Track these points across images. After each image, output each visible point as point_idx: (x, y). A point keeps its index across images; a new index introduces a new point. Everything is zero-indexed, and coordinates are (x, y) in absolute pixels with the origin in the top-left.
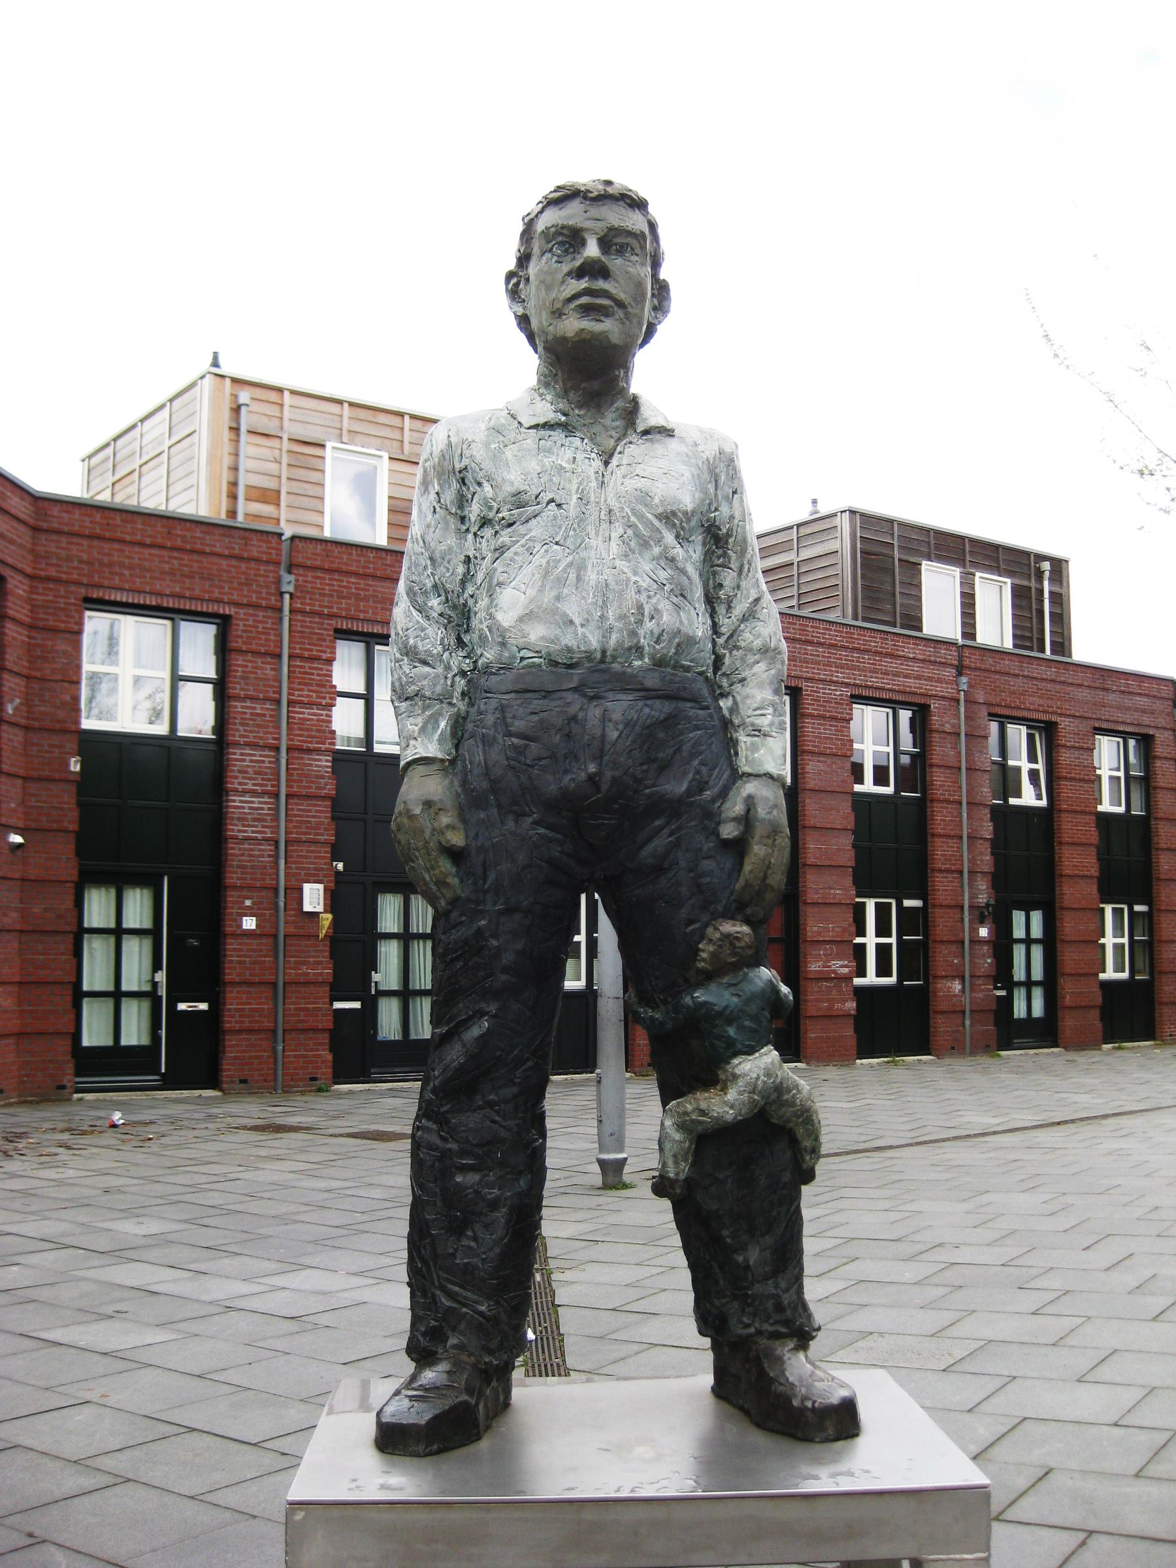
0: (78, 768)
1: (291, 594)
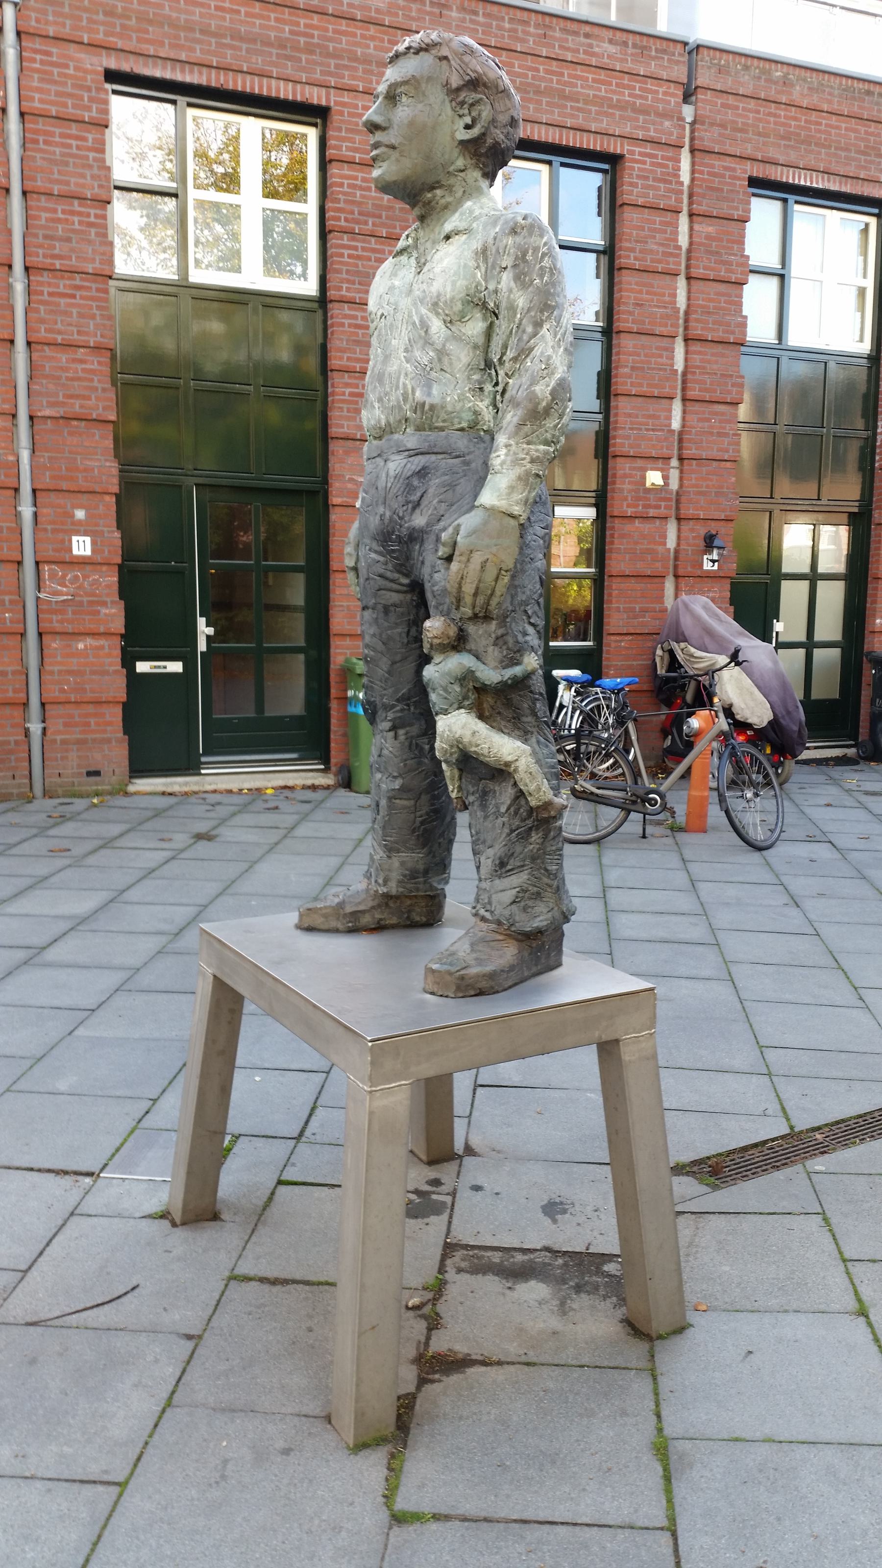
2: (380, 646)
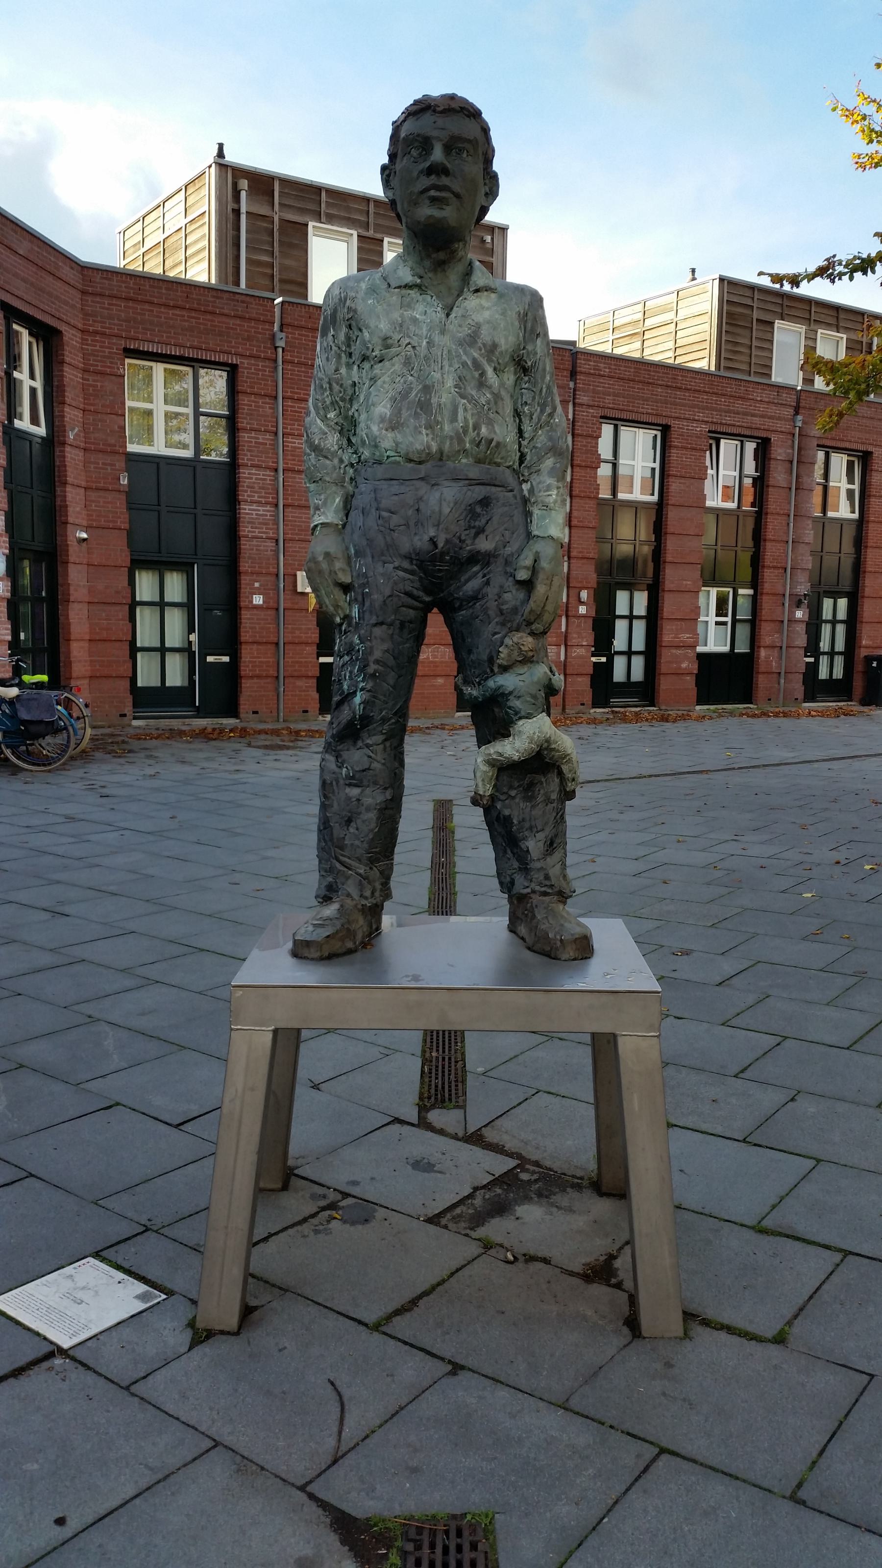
0: (126, 482)
1: (283, 349)
2: (391, 662)
